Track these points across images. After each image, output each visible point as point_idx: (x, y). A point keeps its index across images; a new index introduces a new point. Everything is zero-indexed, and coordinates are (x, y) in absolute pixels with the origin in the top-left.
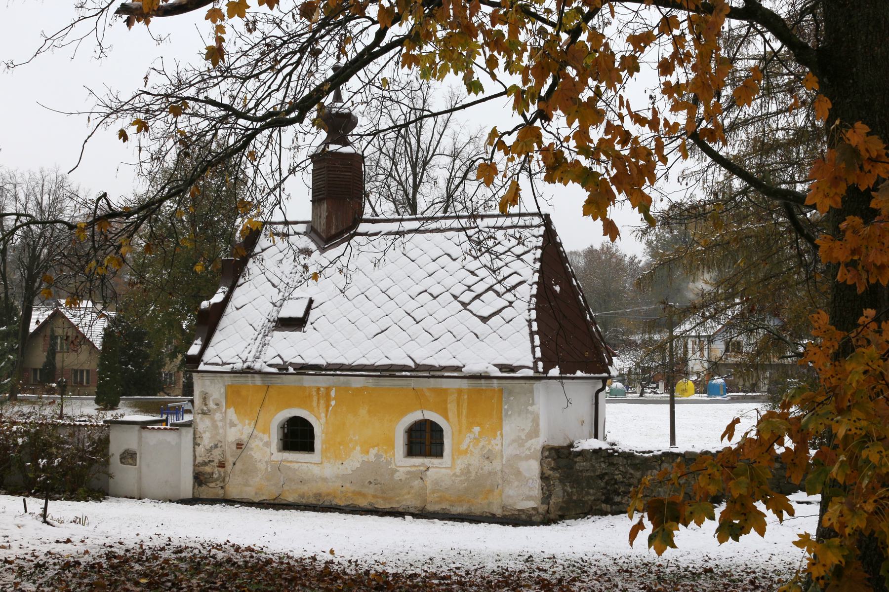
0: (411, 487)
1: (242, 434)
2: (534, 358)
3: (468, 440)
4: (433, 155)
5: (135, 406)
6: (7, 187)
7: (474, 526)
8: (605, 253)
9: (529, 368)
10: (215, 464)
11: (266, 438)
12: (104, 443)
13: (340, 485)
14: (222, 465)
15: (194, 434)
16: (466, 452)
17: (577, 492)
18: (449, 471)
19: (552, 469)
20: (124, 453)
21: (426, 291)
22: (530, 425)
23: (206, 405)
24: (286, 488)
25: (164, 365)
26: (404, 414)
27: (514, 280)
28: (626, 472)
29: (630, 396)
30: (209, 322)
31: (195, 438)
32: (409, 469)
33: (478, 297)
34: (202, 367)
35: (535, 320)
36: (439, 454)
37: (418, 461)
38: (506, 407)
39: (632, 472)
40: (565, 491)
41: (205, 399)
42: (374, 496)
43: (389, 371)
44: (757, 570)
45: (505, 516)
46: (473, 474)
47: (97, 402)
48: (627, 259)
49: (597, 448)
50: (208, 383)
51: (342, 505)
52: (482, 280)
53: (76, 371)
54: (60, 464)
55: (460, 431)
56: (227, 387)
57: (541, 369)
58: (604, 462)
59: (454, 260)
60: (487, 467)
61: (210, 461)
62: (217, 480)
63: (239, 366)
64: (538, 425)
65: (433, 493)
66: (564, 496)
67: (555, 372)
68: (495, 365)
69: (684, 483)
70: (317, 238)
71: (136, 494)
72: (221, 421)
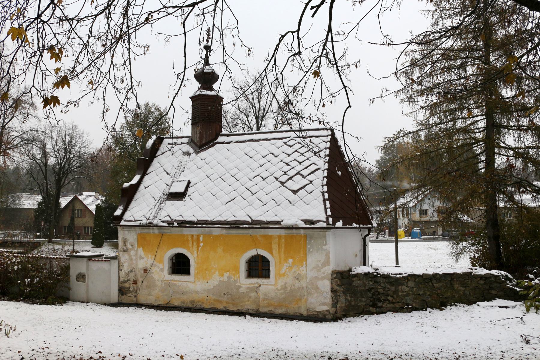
0: (250, 297)
1: (147, 264)
2: (326, 215)
3: (284, 268)
4: (267, 112)
5: (112, 246)
10: (131, 282)
11: (161, 266)
12: (66, 270)
14: (135, 283)
15: (119, 263)
16: (284, 275)
17: (354, 300)
18: (273, 287)
19: (338, 285)
20: (78, 275)
21: (258, 175)
23: (125, 246)
24: (173, 297)
27: (313, 167)
28: (385, 287)
30: (129, 195)
31: (119, 266)
32: (248, 286)
33: (291, 178)
34: (122, 223)
36: (267, 276)
38: (309, 247)
39: (389, 287)
40: (346, 299)
42: (227, 303)
43: (235, 225)
45: (308, 316)
46: (289, 289)
47: (92, 243)
48: (367, 169)
49: (367, 272)
50: (126, 232)
52: (293, 168)
53: (85, 227)
54: (37, 282)
57: (331, 222)
58: (371, 281)
59: (276, 157)
60: (298, 284)
61: (128, 280)
62: (132, 291)
63: (144, 222)
64: (329, 258)
66: (346, 303)
67: (340, 224)
68: (302, 220)
69: (422, 294)
71: (85, 300)
72: (134, 256)
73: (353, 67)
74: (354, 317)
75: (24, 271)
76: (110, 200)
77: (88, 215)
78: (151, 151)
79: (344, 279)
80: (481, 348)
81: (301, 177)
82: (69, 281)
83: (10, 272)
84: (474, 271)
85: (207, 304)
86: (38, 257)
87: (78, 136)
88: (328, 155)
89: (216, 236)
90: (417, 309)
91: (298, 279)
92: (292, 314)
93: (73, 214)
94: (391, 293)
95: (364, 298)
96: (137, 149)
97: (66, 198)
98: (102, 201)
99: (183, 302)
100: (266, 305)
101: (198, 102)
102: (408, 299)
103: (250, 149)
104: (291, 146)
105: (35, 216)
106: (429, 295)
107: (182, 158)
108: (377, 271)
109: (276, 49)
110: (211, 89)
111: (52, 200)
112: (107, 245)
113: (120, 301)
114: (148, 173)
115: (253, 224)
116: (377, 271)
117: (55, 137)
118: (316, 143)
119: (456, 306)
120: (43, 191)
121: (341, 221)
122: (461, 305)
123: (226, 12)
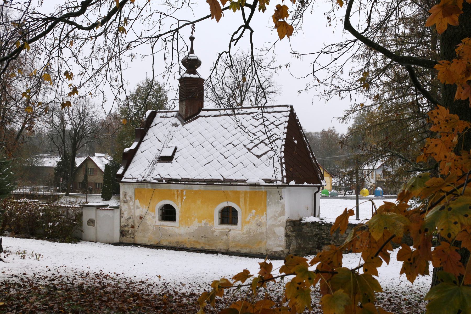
2: (282, 176)
3: (249, 217)
4: (249, 87)
7: (251, 259)
8: (330, 133)
9: (279, 181)
10: (130, 226)
11: (153, 214)
12: (79, 217)
14: (133, 227)
15: (120, 212)
18: (240, 232)
19: (291, 231)
24: (162, 238)
26: (218, 203)
28: (328, 234)
29: (339, 196)
30: (128, 158)
31: (120, 214)
32: (221, 230)
34: (123, 180)
35: (283, 157)
37: (225, 226)
40: (297, 242)
42: (204, 244)
43: (211, 182)
44: (393, 291)
46: (252, 233)
47: (102, 197)
48: (340, 136)
49: (314, 221)
50: (126, 187)
53: (96, 183)
54: (58, 225)
55: (246, 212)
57: (285, 182)
58: (317, 228)
60: (259, 230)
62: (131, 234)
63: (140, 179)
64: (284, 209)
67: (293, 183)
68: (262, 179)
70: (181, 119)
71: (94, 240)
73: (284, 68)
75: (48, 217)
76: (117, 160)
77: (99, 173)
79: (295, 226)
80: (388, 278)
83: (37, 218)
88: (287, 128)
89: (196, 191)
93: (87, 172)
94: (333, 238)
97: (80, 158)
98: (111, 162)
99: (170, 243)
103: (225, 121)
104: (258, 120)
105: (55, 174)
108: (322, 221)
109: (217, 63)
110: (195, 73)
111: (69, 160)
113: (121, 241)
116: (322, 221)
120: (62, 153)
123: (180, 40)
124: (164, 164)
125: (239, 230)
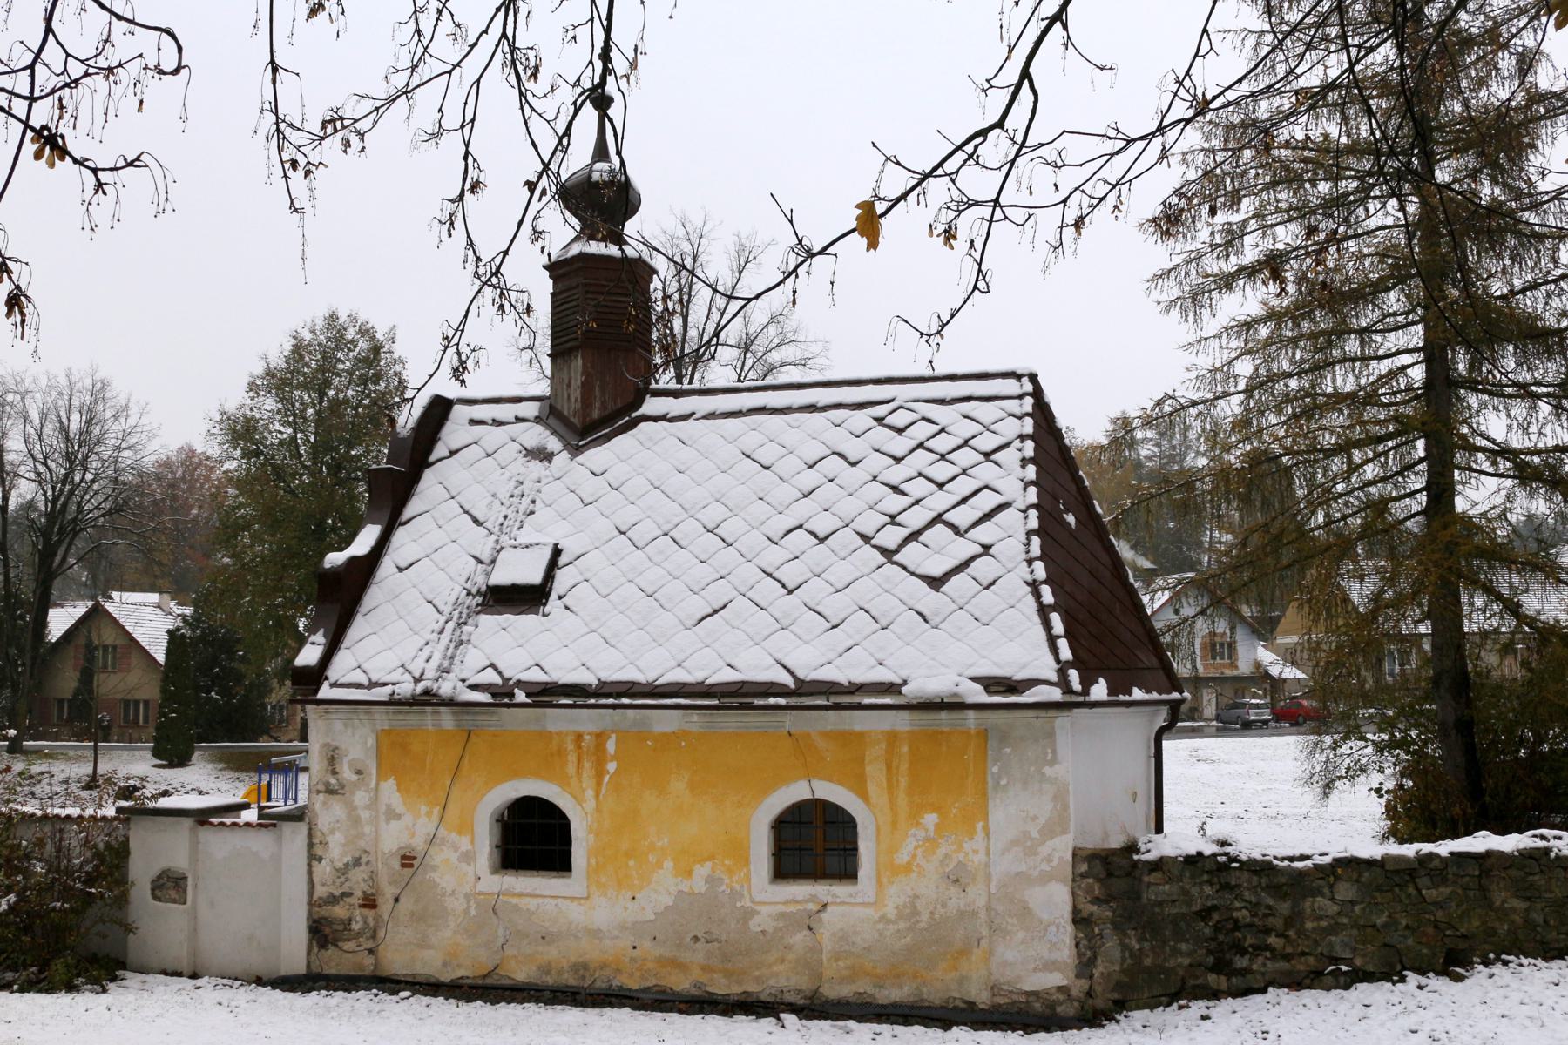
0: (788, 948)
1: (413, 835)
2: (1058, 661)
3: (910, 844)
5: (220, 760)
6: (10, 397)
10: (354, 901)
11: (464, 843)
12: (112, 861)
13: (629, 944)
14: (370, 903)
15: (310, 835)
16: (907, 869)
17: (1152, 949)
18: (870, 911)
19: (1097, 901)
20: (159, 877)
21: (800, 527)
22: (1050, 806)
23: (334, 773)
24: (509, 951)
25: (271, 691)
27: (987, 501)
28: (1257, 904)
30: (342, 596)
31: (310, 845)
32: (781, 908)
33: (914, 536)
34: (325, 692)
36: (847, 872)
37: (800, 891)
38: (995, 769)
39: (1270, 902)
40: (1125, 947)
41: (332, 761)
43: (738, 696)
45: (996, 1008)
46: (925, 917)
47: (156, 753)
49: (1193, 851)
50: (338, 725)
51: (636, 987)
52: (917, 502)
53: (127, 703)
55: (894, 824)
56: (380, 735)
57: (1077, 686)
59: (854, 464)
60: (956, 900)
61: (344, 895)
62: (359, 934)
63: (406, 688)
64: (1066, 807)
65: (837, 960)
66: (1123, 959)
67: (1099, 691)
68: (974, 679)
69: (1385, 925)
71: (185, 967)
72: (368, 807)
74: (1152, 1008)
77: (135, 659)
78: (413, 449)
81: (950, 532)
82: (127, 902)
84: (1553, 843)
85: (631, 975)
86: (10, 818)
87: (109, 414)
88: (1033, 460)
89: (664, 734)
90: (1369, 977)
91: (957, 881)
92: (937, 1002)
94: (1277, 922)
95: (1187, 941)
96: (300, 456)
99: (546, 969)
100: (845, 973)
101: (574, 282)
102: (1338, 943)
104: (900, 431)
106: (1407, 927)
107: (522, 470)
110: (619, 240)
112: (203, 758)
113: (315, 969)
114: (404, 517)
115: (800, 695)
117: (34, 415)
118: (986, 420)
119: (1506, 963)
121: (1101, 680)
122: (1524, 961)
124: (507, 619)
125: (863, 904)
